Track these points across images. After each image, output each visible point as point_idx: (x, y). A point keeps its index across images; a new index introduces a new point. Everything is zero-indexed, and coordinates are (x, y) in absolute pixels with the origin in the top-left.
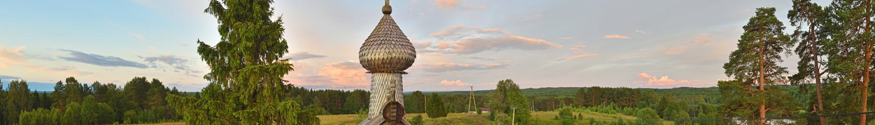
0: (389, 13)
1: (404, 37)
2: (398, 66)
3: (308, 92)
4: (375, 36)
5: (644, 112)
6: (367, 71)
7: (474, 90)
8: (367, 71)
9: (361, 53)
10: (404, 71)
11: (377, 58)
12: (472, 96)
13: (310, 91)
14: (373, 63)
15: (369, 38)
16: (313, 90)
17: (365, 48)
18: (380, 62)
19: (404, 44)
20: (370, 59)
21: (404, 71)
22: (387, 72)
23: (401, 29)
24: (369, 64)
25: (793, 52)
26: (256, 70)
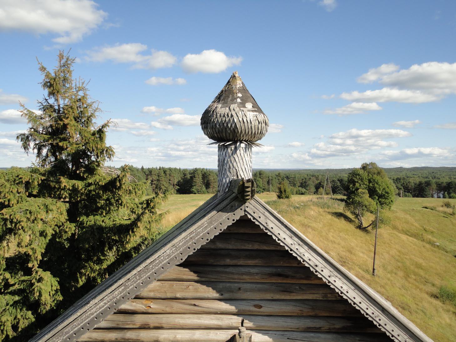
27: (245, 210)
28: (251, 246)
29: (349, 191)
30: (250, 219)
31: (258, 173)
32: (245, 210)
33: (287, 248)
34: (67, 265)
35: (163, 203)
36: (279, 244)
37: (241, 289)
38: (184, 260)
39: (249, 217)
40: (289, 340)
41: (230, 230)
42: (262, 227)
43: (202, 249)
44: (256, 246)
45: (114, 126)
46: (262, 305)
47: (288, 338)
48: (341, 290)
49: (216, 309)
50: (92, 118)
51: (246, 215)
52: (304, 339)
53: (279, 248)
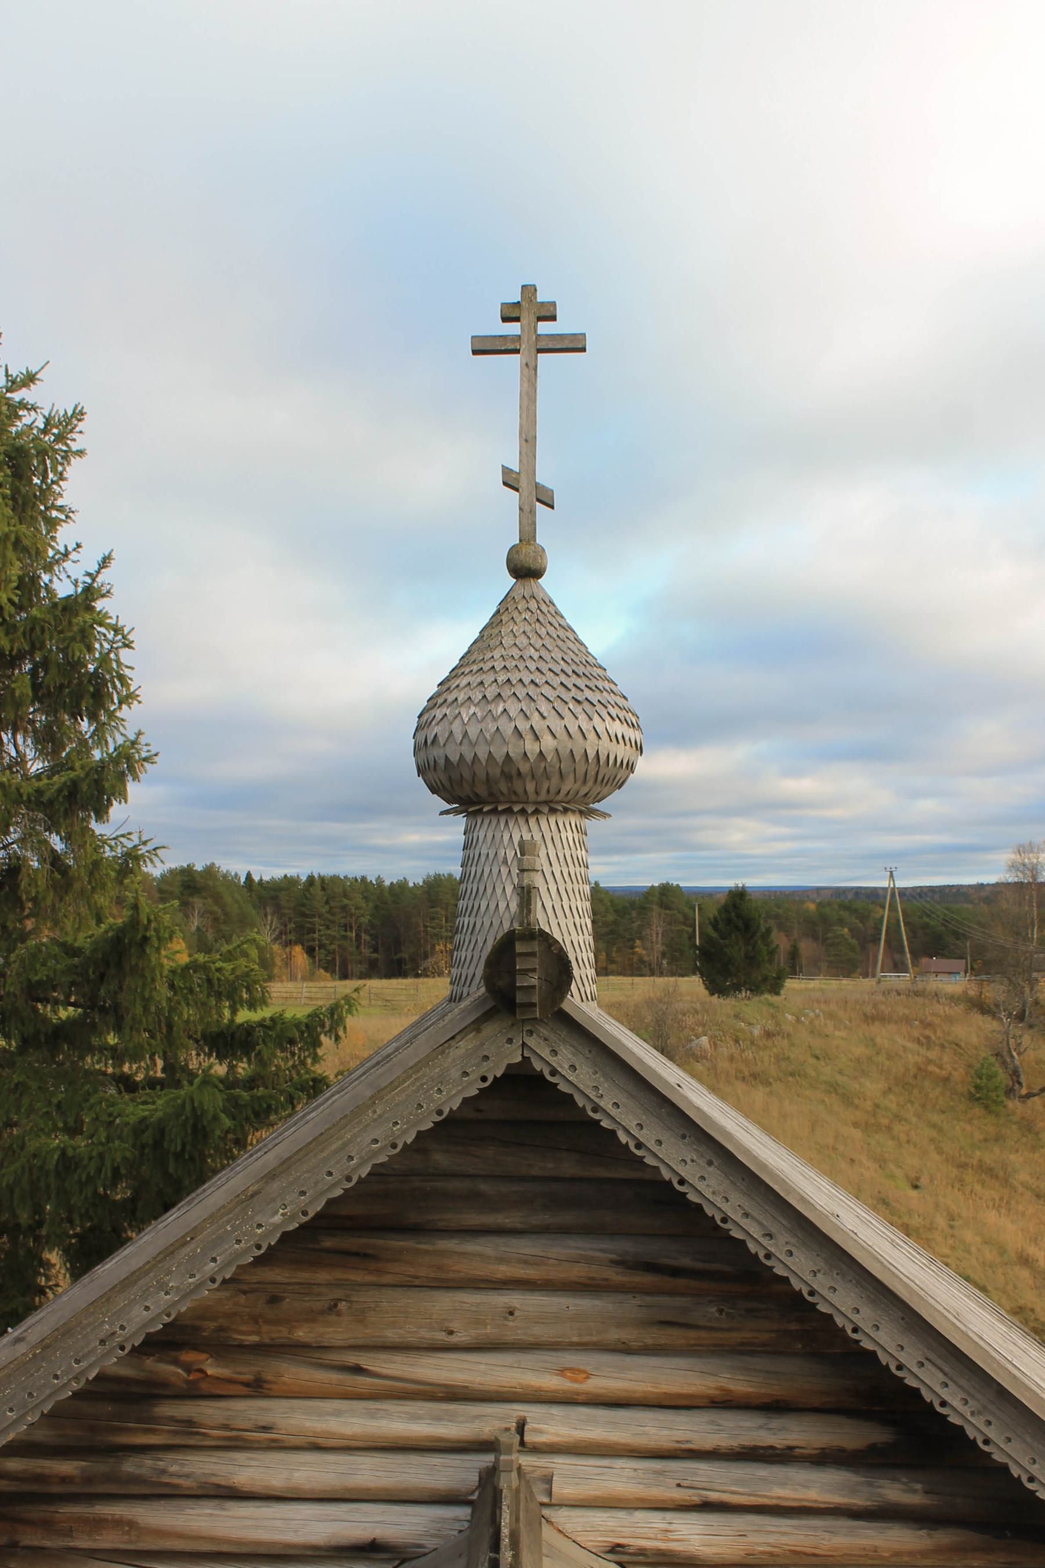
0: (536, 574)
1: (607, 685)
2: (565, 789)
3: (237, 885)
4: (475, 668)
5: (159, 1002)
6: (448, 807)
7: (901, 883)
8: (448, 807)
9: (421, 737)
10: (596, 806)
11: (483, 756)
12: (893, 908)
13: (243, 880)
14: (467, 775)
15: (455, 673)
16: (256, 878)
17: (439, 713)
18: (495, 772)
19: (594, 697)
20: (454, 758)
21: (596, 806)
22: (523, 812)
23: (581, 637)
24: (450, 779)
25: (783, 997)
26: (651, 957)
27: (523, 1043)
28: (550, 1165)
29: (735, 981)
30: (540, 1076)
31: (318, 883)
32: (523, 1043)
33: (666, 1175)
34: (39, 1009)
35: (57, 535)
36: (640, 1160)
37: (517, 1313)
38: (311, 1214)
39: (538, 1066)
40: (680, 1489)
41: (481, 1111)
42: (580, 1102)
43: (377, 1173)
44: (569, 1167)
45: (257, 933)
46: (589, 1369)
47: (679, 1485)
48: (855, 1317)
49: (452, 1442)
50: (114, 802)
51: (526, 1060)
52: (733, 1489)
53: (646, 1175)
